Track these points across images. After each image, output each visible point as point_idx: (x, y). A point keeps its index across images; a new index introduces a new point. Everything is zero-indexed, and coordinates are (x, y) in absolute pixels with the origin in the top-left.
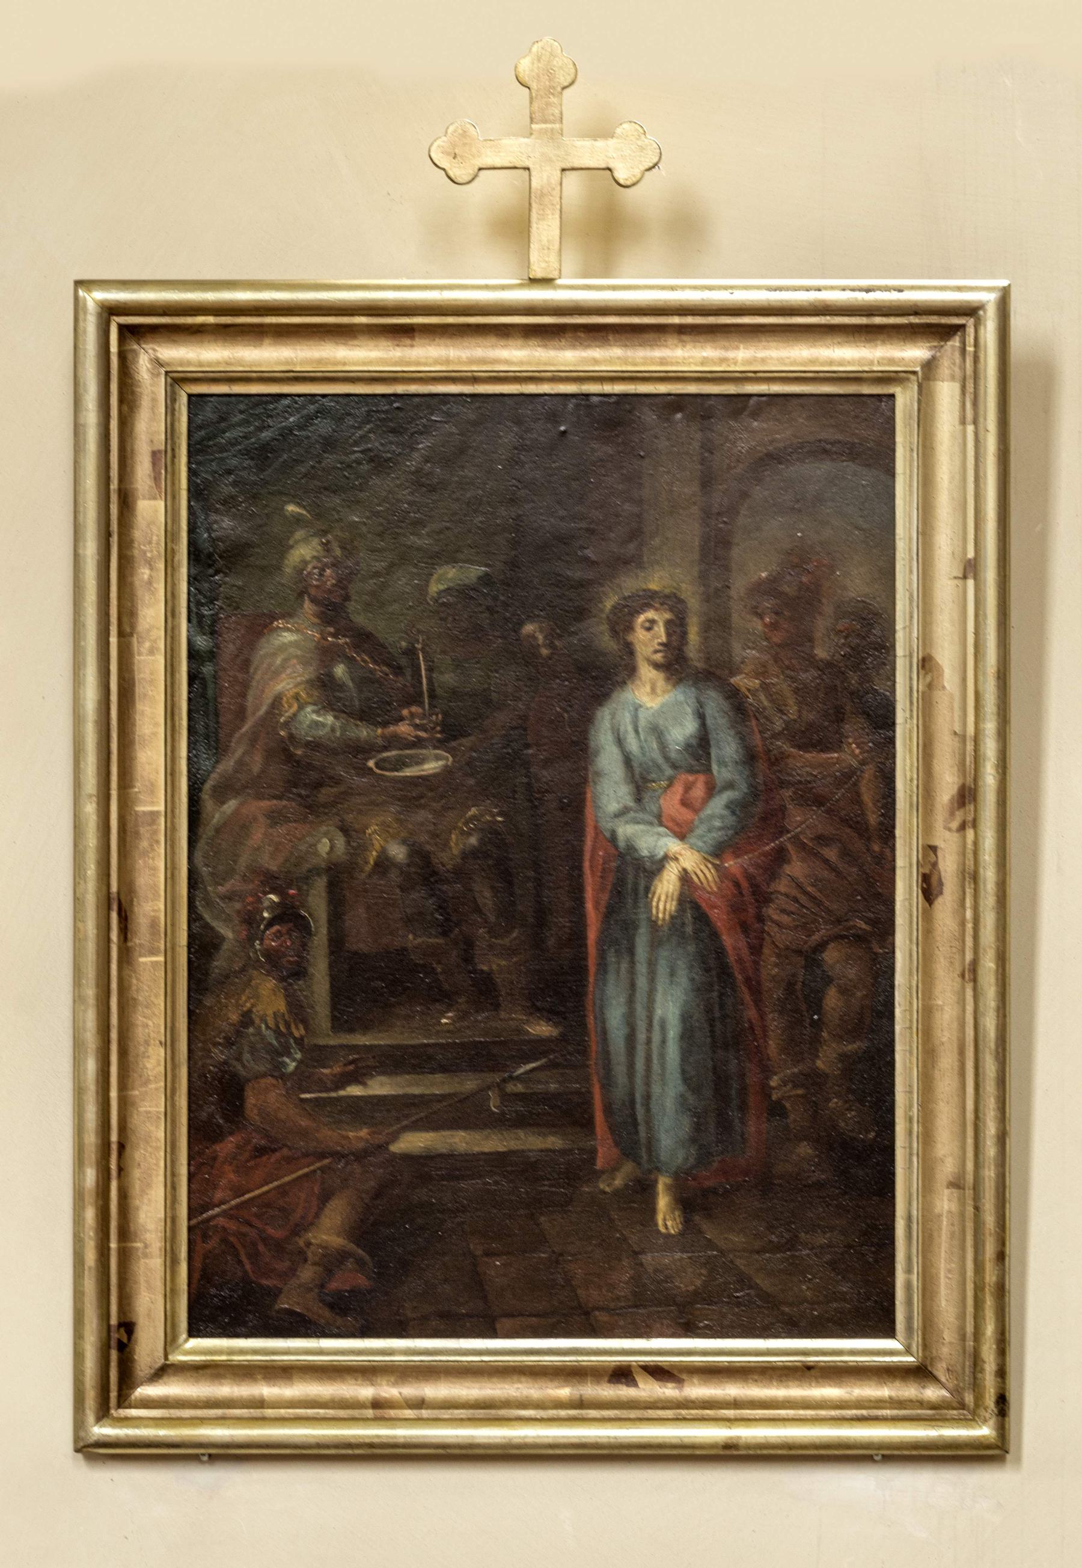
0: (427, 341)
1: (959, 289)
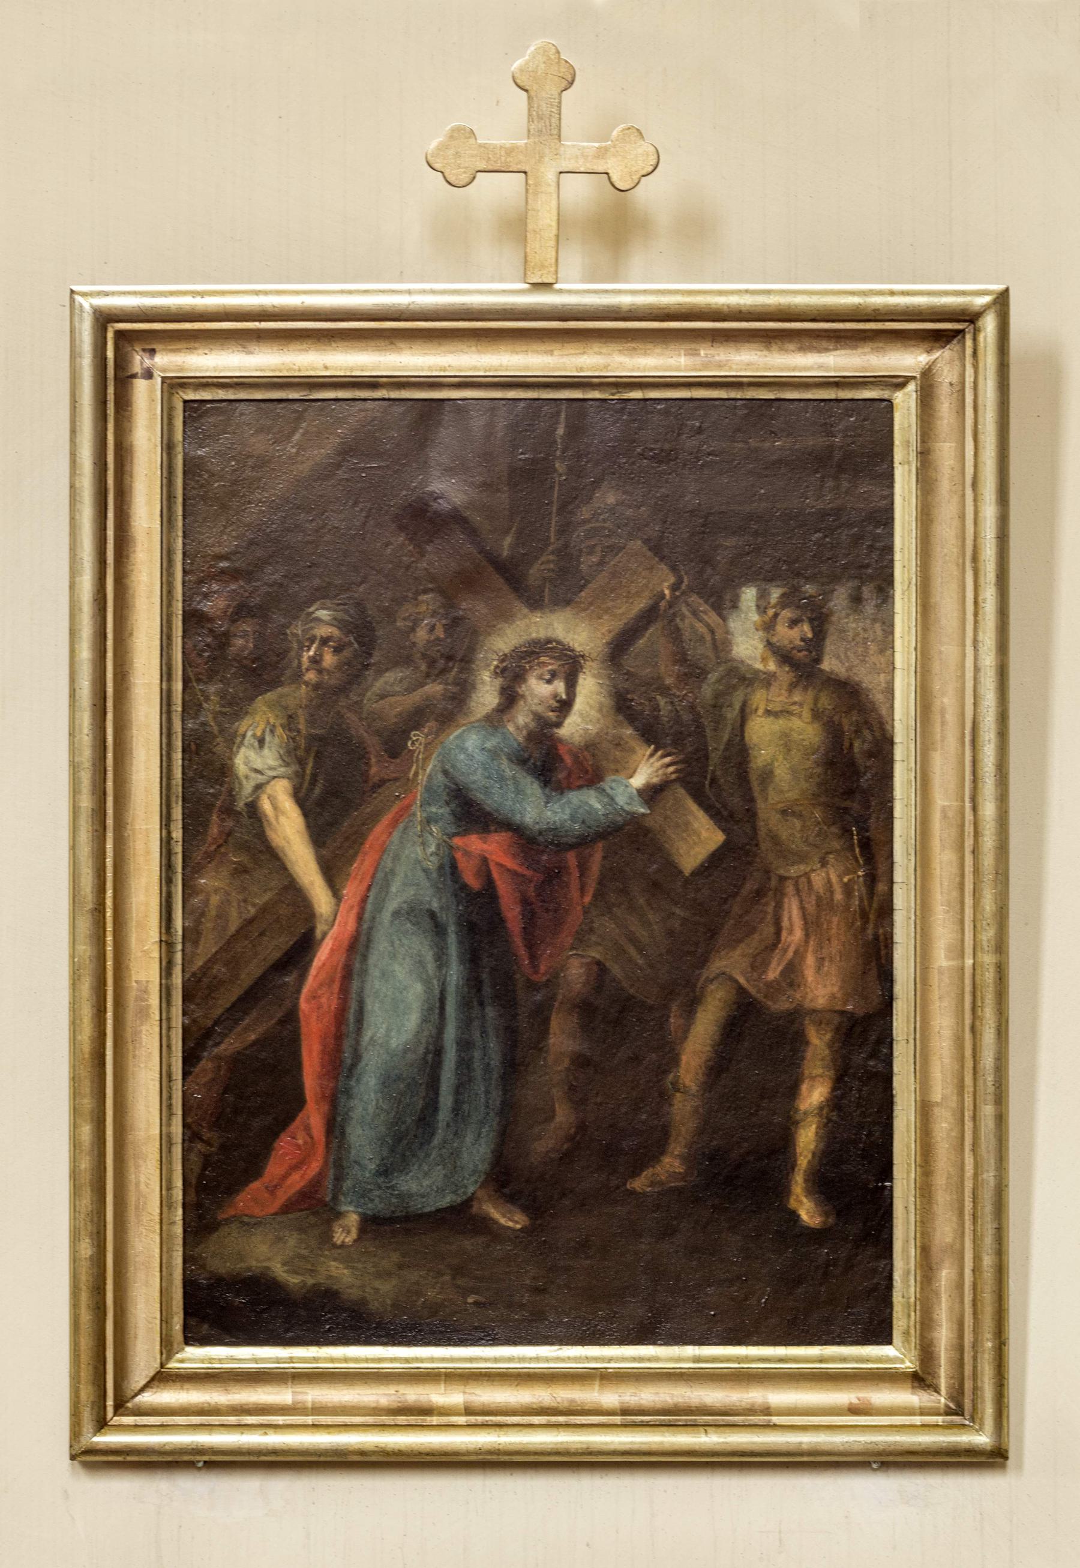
0: (464, 347)
1: (257, 293)
